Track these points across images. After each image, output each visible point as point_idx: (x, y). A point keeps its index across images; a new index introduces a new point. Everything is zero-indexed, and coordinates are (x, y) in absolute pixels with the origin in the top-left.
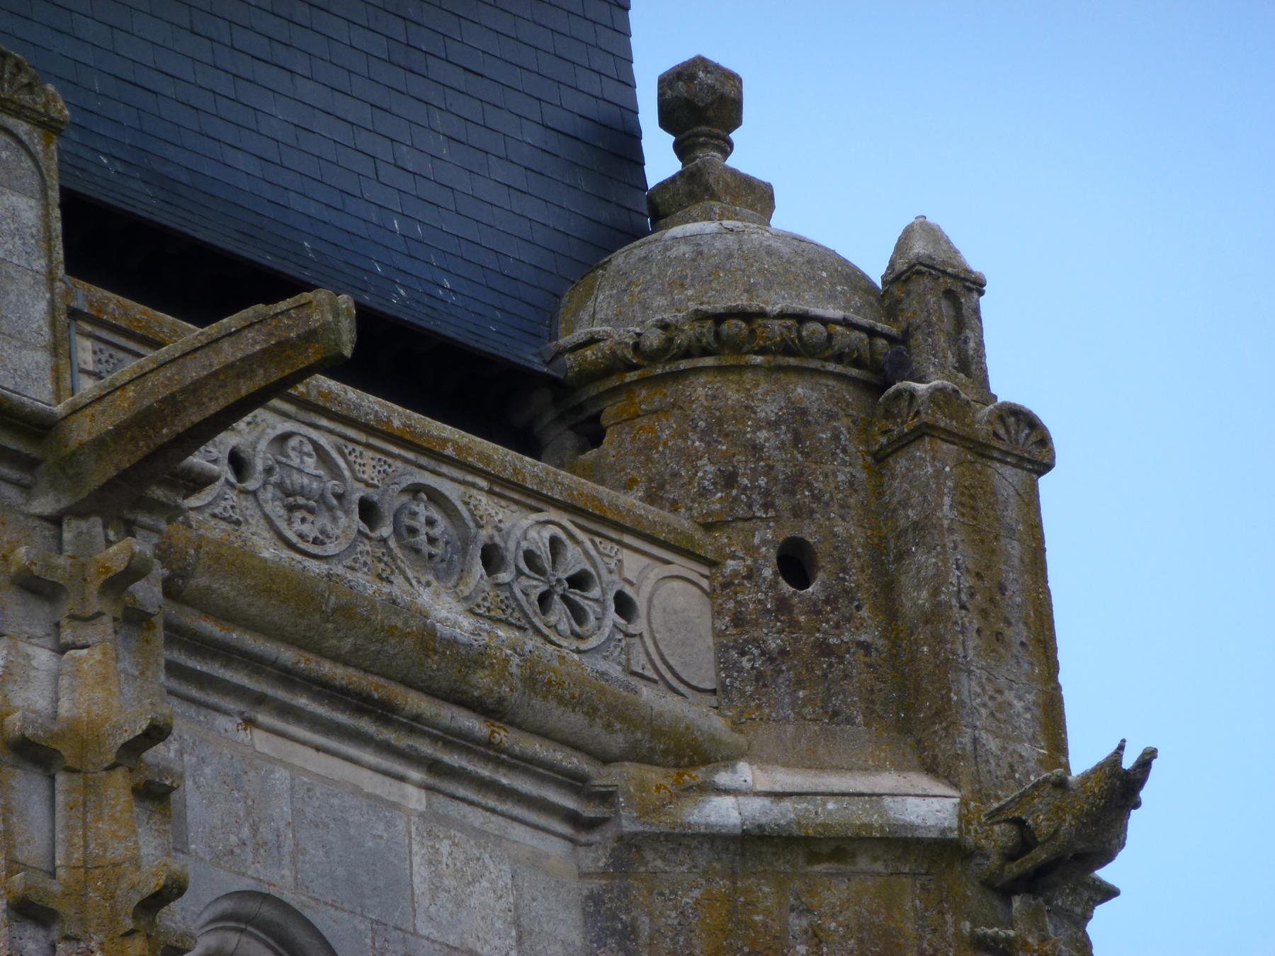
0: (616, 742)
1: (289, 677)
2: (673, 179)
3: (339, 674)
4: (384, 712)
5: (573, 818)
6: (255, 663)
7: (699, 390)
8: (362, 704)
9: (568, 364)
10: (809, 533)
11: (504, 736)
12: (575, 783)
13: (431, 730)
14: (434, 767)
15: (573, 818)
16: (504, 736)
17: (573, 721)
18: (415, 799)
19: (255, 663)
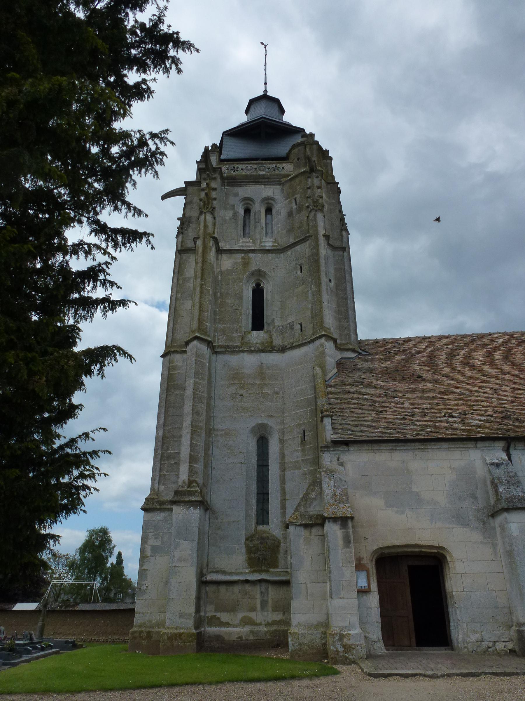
0: (281, 177)
1: (248, 182)
2: (262, 95)
3: (253, 180)
4: (258, 182)
5: (279, 184)
6: (245, 182)
7: (293, 152)
8: (256, 182)
9: (95, 147)
10: (299, 157)
11: (270, 180)
12: (278, 181)
13: (51, 651)
14: (264, 184)
15: (279, 184)
16: (270, 180)
17: (276, 177)
18: (263, 187)
19: (245, 182)
